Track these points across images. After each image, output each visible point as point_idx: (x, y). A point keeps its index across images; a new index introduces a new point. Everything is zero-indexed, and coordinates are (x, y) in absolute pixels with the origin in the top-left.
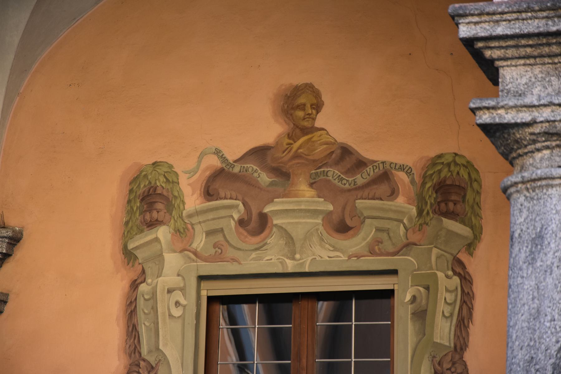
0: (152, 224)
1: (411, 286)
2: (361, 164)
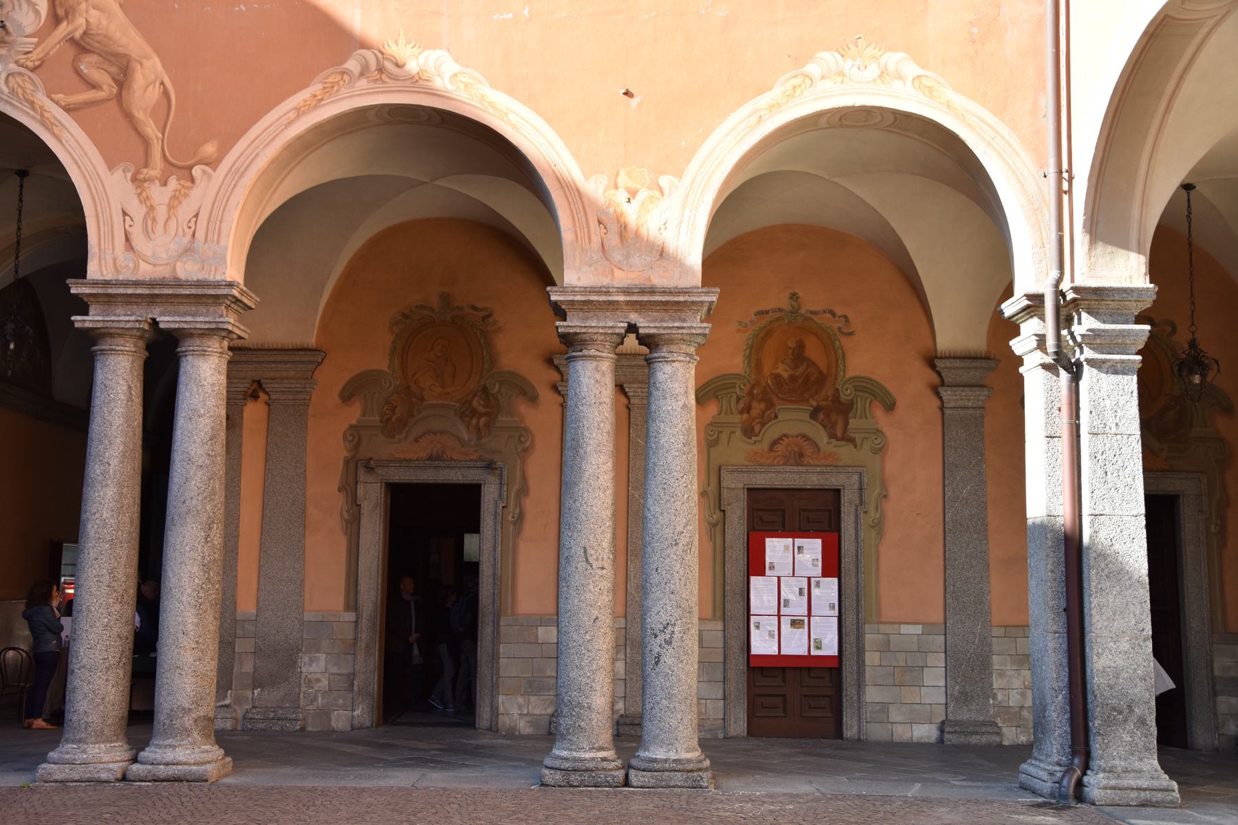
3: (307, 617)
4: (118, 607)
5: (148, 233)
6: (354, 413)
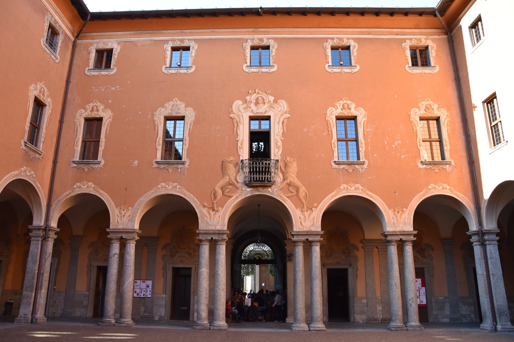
5: (305, 222)
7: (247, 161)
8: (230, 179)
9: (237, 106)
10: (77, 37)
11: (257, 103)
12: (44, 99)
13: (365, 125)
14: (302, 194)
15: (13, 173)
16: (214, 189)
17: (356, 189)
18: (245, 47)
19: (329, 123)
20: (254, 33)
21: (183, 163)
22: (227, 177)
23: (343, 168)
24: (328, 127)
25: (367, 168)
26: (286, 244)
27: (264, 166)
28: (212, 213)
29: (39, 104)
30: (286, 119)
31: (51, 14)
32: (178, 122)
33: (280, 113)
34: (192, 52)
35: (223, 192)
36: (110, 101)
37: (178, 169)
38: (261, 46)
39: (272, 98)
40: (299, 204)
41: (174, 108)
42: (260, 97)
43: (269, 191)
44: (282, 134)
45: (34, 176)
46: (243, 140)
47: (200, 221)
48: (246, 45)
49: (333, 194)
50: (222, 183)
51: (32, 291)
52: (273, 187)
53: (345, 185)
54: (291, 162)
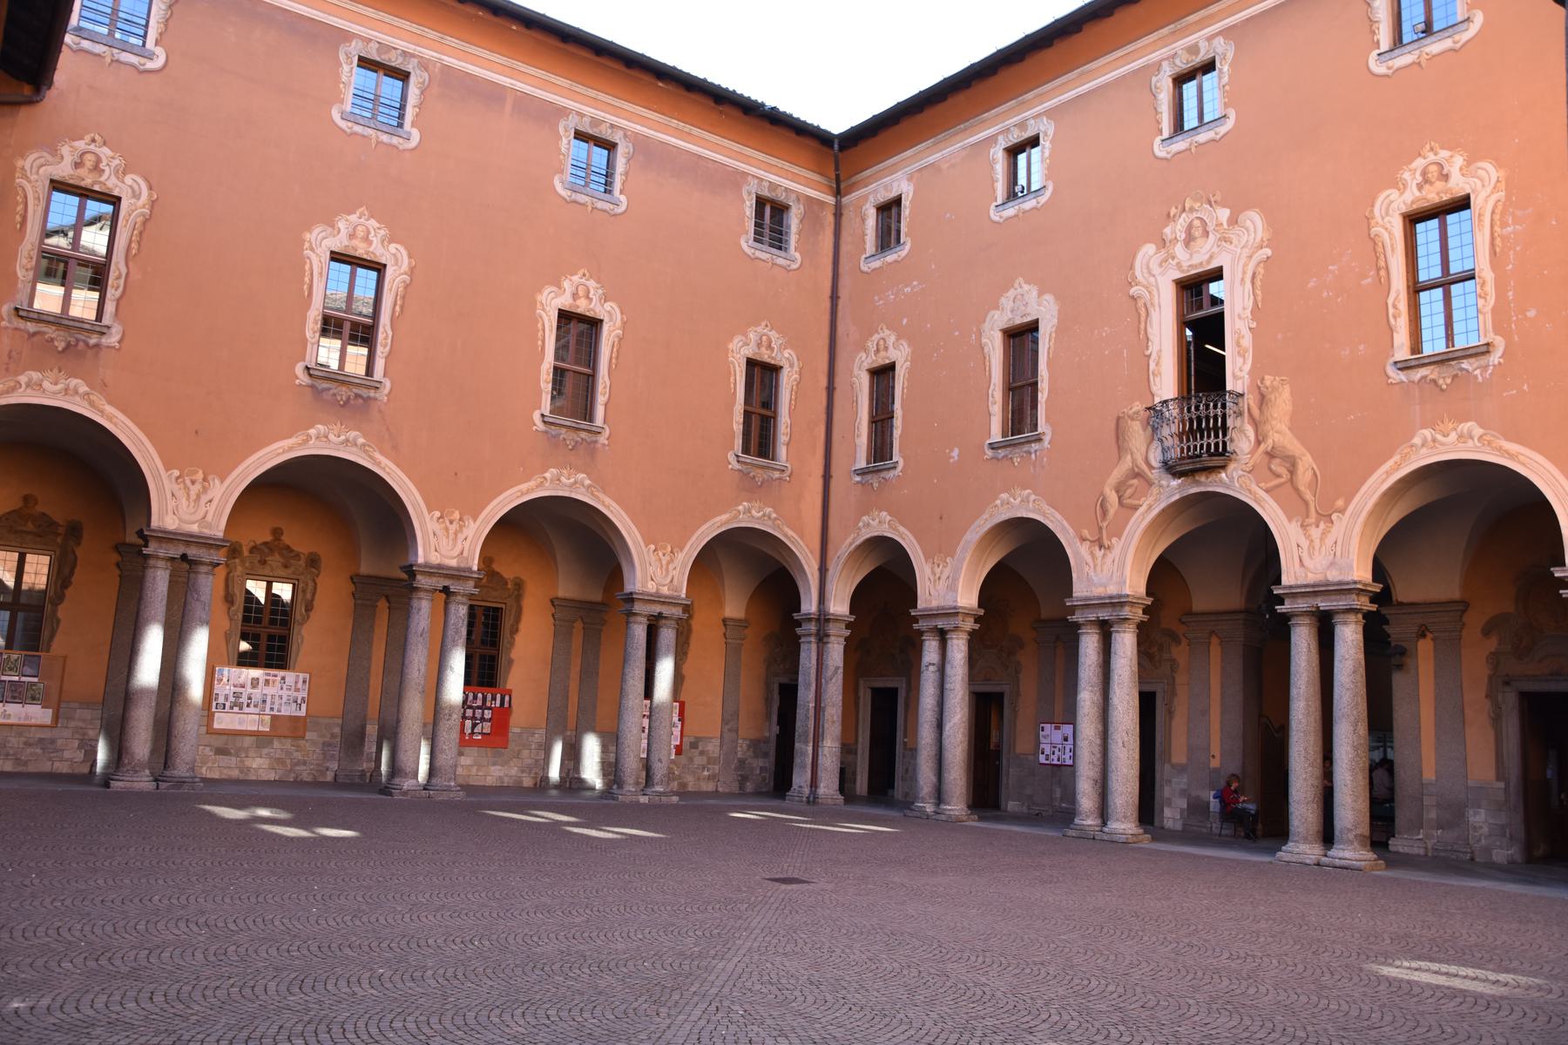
0: (234, 558)
1: (760, 456)
2: (292, 551)
3: (1470, 783)
4: (1310, 769)
5: (1311, 556)
6: (1492, 644)
7: (1173, 411)
8: (1134, 461)
9: (1144, 262)
10: (838, 193)
11: (1189, 240)
12: (592, 306)
13: (1497, 217)
14: (1304, 477)
15: (718, 519)
16: (1102, 494)
17: (1462, 440)
18: (1156, 87)
19: (1380, 244)
20: (1164, 42)
21: (1039, 440)
22: (1129, 457)
23: (1424, 378)
24: (1377, 258)
25: (1500, 363)
26: (1388, 617)
27: (1194, 417)
28: (1099, 553)
29: (762, 374)
30: (1262, 265)
31: (757, 178)
32: (1451, 218)
33: (1246, 252)
34: (1220, 70)
35: (1120, 498)
36: (905, 321)
37: (1030, 453)
38: (1197, 66)
39: (1224, 214)
40: (1298, 508)
41: (1018, 303)
42: (1198, 218)
43: (1221, 481)
44: (1252, 312)
45: (774, 515)
46: (1161, 351)
47: (1074, 576)
48: (1158, 81)
49: (1390, 463)
50: (1117, 474)
51: (806, 743)
52: (1232, 466)
53: (1427, 433)
54: (1275, 389)
